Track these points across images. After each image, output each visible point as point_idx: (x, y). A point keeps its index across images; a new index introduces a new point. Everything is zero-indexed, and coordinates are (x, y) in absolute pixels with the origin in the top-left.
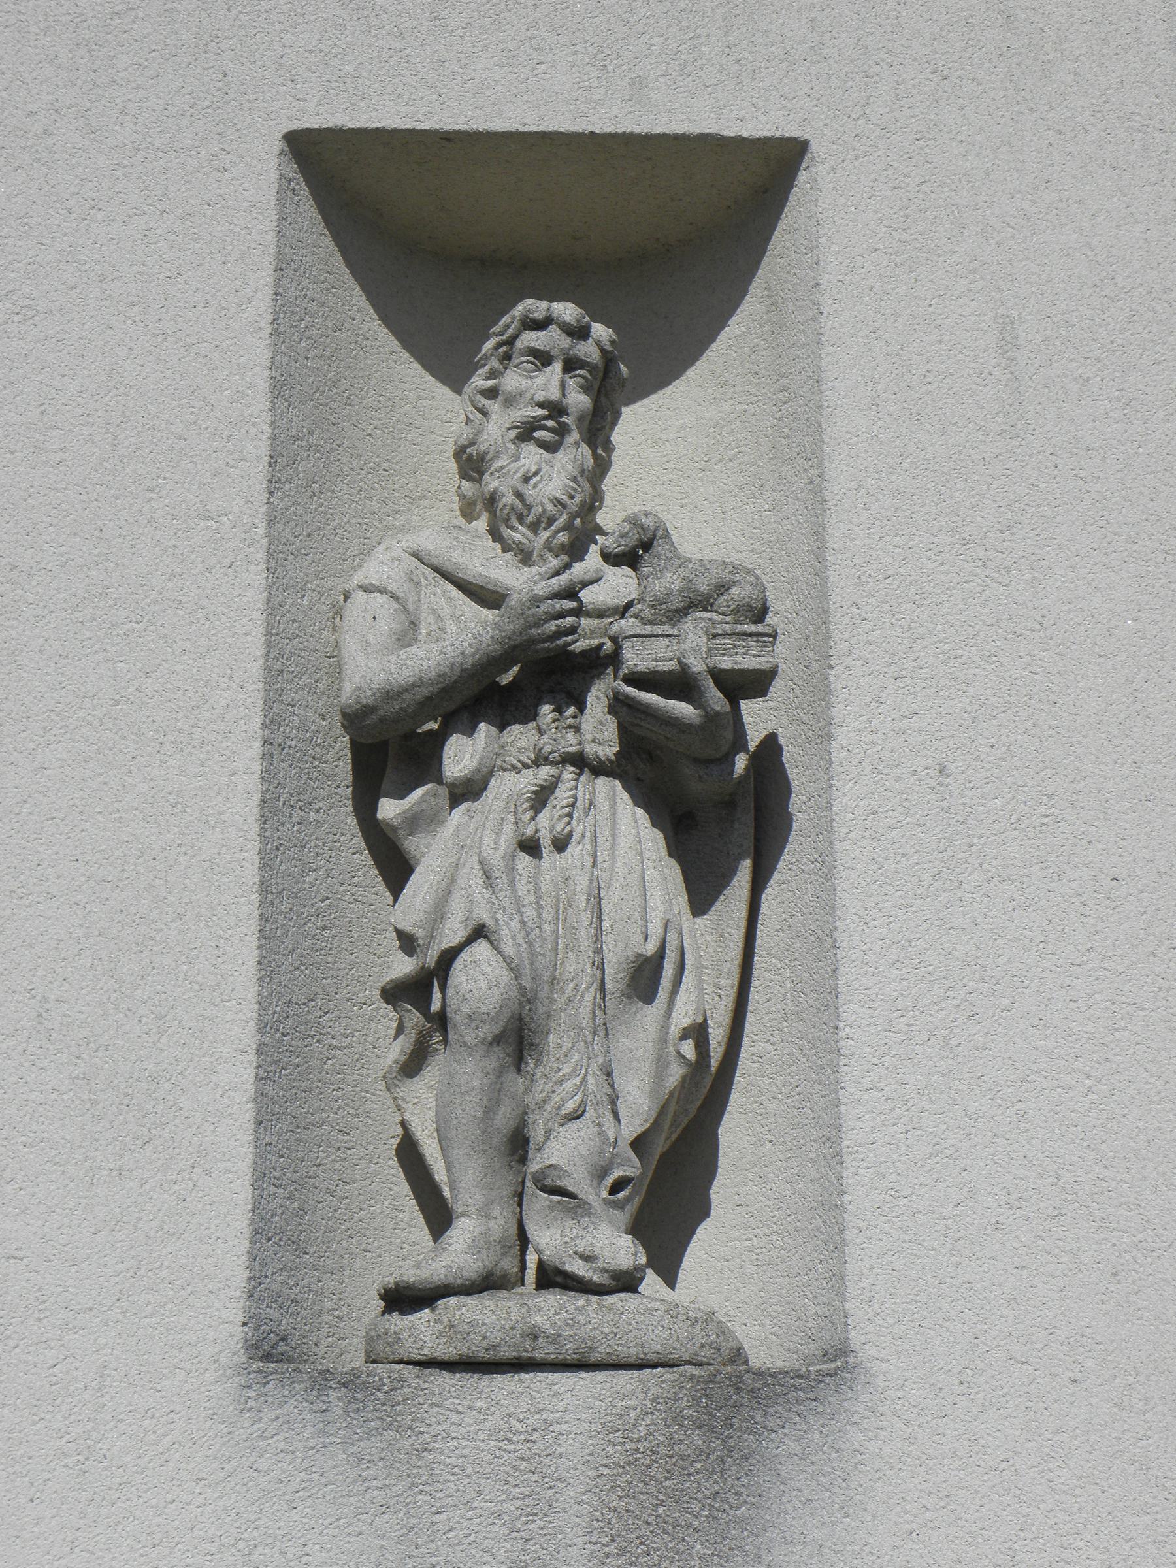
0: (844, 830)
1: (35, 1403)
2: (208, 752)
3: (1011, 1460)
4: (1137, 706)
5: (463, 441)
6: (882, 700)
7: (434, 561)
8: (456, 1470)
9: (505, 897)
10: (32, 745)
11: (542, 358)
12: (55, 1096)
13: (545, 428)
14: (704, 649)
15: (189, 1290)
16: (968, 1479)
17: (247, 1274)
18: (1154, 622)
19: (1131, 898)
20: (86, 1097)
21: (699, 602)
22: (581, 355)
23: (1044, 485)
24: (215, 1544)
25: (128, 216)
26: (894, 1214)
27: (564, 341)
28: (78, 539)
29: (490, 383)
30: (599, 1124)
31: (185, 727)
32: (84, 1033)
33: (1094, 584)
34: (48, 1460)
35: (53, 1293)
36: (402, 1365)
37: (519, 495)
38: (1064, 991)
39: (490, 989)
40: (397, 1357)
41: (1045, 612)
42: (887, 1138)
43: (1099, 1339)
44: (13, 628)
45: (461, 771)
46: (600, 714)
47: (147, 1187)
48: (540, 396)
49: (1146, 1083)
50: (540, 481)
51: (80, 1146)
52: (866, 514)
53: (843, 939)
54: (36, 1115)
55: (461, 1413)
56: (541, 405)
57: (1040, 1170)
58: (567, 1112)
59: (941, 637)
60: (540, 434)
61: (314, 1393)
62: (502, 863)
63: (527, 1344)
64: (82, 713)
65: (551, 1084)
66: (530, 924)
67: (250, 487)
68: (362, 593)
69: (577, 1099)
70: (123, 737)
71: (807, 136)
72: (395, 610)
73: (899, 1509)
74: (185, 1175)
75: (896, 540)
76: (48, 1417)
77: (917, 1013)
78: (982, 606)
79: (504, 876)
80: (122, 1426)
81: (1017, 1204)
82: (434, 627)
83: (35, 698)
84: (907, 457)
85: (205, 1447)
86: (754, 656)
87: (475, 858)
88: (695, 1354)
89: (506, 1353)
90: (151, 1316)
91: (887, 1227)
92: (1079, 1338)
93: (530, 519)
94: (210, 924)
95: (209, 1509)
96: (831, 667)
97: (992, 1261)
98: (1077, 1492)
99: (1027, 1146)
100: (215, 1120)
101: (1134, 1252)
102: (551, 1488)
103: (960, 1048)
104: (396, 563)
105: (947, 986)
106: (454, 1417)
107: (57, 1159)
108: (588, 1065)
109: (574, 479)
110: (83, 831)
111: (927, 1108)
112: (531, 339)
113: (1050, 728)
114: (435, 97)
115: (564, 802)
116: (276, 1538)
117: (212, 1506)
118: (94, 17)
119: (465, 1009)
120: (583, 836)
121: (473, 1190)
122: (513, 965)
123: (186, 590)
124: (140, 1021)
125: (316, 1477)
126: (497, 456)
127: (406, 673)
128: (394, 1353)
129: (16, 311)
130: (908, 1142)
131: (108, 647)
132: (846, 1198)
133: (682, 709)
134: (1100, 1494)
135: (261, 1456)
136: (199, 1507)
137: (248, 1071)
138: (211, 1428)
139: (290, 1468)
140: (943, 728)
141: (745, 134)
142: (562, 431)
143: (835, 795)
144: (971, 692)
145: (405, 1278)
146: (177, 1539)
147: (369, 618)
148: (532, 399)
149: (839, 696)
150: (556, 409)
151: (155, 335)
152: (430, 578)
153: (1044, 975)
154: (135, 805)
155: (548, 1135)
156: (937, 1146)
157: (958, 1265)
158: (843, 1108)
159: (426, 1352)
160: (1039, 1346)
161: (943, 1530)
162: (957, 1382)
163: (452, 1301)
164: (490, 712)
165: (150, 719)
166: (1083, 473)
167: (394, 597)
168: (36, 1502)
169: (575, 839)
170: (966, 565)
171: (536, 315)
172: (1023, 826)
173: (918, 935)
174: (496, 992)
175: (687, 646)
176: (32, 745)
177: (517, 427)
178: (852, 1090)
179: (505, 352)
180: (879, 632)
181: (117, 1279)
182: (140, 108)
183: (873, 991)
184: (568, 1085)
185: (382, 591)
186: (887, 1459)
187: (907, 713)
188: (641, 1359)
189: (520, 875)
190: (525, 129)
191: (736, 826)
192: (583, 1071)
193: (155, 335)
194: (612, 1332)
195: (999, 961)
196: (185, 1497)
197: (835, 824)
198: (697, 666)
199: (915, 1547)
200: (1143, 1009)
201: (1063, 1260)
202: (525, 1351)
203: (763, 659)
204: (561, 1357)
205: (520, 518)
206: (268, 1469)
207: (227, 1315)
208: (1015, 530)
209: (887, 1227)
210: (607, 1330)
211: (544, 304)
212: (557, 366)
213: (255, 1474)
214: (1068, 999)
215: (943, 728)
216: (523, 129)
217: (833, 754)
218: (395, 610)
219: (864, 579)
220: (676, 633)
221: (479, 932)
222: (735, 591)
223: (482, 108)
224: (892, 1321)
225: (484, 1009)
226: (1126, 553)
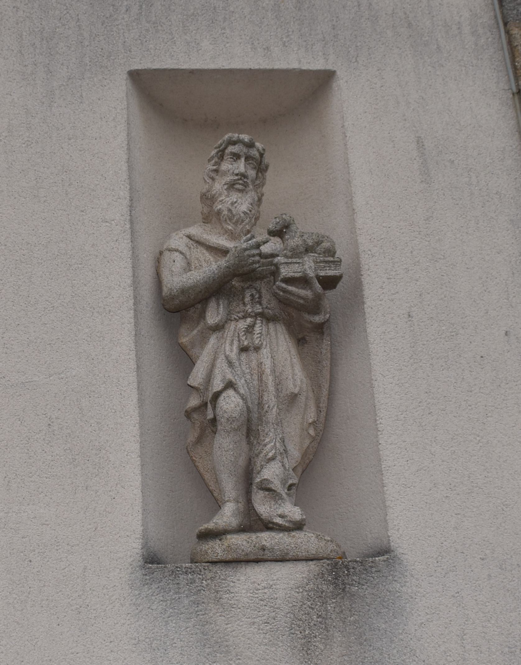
0: (373, 340)
1: (58, 584)
2: (112, 315)
3: (460, 593)
4: (485, 288)
5: (204, 191)
6: (384, 287)
7: (196, 238)
8: (234, 606)
9: (238, 370)
10: (40, 315)
11: (236, 157)
12: (58, 457)
13: (240, 184)
14: (313, 268)
15: (119, 535)
16: (443, 601)
17: (142, 528)
18: (488, 255)
19: (489, 364)
20: (70, 457)
21: (308, 250)
22: (252, 155)
23: (440, 202)
24: (137, 640)
25: (67, 104)
26: (405, 494)
27: (245, 150)
28: (54, 232)
29: (215, 167)
30: (282, 462)
31: (102, 305)
32: (69, 431)
33: (463, 240)
34: (64, 608)
35: (62, 539)
36: (209, 564)
37: (230, 210)
38: (465, 402)
39: (236, 407)
40: (206, 560)
41: (445, 251)
42: (400, 464)
43: (491, 542)
44: (29, 268)
45: (214, 321)
46: (269, 297)
47: (98, 494)
48: (236, 171)
49: (501, 438)
50: (237, 205)
51: (69, 478)
52: (371, 214)
53: (376, 384)
54: (50, 465)
55: (234, 582)
56: (237, 175)
57: (462, 474)
58: (269, 457)
59: (405, 262)
60: (237, 186)
61: (173, 576)
62: (235, 357)
63: (261, 552)
64: (59, 301)
65: (261, 446)
66: (248, 381)
67: (122, 209)
68: (168, 252)
69: (273, 451)
70: (77, 311)
71: (335, 69)
72: (182, 258)
73: (416, 614)
74: (113, 488)
75: (384, 225)
76: (63, 590)
77: (407, 413)
78: (420, 250)
79: (237, 362)
80: (94, 593)
81: (454, 489)
82: (198, 265)
83: (40, 296)
84: (385, 192)
85: (129, 600)
86: (333, 270)
87: (223, 356)
88: (329, 555)
89: (252, 557)
90: (103, 547)
91: (403, 500)
92: (483, 542)
93: (234, 221)
94: (118, 385)
95: (133, 626)
96: (362, 275)
97: (446, 512)
98: (487, 604)
99: (456, 465)
100: (124, 465)
101: (502, 506)
102: (274, 612)
103: (426, 426)
104: (181, 240)
105: (419, 402)
106: (232, 584)
107: (60, 483)
108: (276, 438)
109: (251, 204)
110: (62, 349)
111: (415, 451)
112: (231, 149)
113: (451, 297)
114: (187, 56)
115: (258, 332)
116: (161, 637)
117: (134, 625)
118: (49, 28)
119: (226, 415)
120: (266, 345)
121: (231, 491)
122: (244, 397)
123: (99, 251)
124: (91, 425)
125: (176, 611)
126: (220, 195)
127: (190, 281)
128: (205, 559)
129: (24, 142)
130: (409, 465)
131: (69, 274)
132: (385, 488)
133: (303, 292)
134: (496, 605)
135: (153, 603)
136: (128, 625)
137: (137, 444)
138: (131, 592)
139: (165, 608)
140: (409, 298)
141: (311, 68)
142: (246, 185)
143: (368, 326)
144: (418, 283)
145: (209, 527)
146: (120, 639)
147: (172, 261)
148: (233, 173)
149: (366, 287)
150: (244, 176)
151: (80, 151)
152: (195, 246)
153: (457, 396)
154: (84, 337)
155: (262, 467)
156: (420, 466)
157: (432, 514)
158: (381, 452)
159: (219, 557)
160: (467, 546)
161: (434, 622)
162: (435, 562)
163: (229, 536)
164: (224, 298)
165: (88, 303)
166: (455, 197)
167: (181, 253)
168: (60, 625)
169: (264, 346)
170: (412, 234)
171: (234, 139)
172: (444, 336)
173: (406, 381)
174: (238, 409)
175: (306, 267)
176: (40, 315)
177: (227, 184)
178: (384, 445)
179: (220, 155)
180: (380, 261)
181: (88, 532)
182: (69, 63)
183: (389, 404)
184: (269, 446)
185: (177, 250)
186: (410, 594)
187: (393, 293)
188: (307, 557)
189: (243, 362)
190: (224, 68)
191: (324, 341)
192: (274, 440)
193: (80, 151)
194: (295, 547)
195: (439, 391)
196: (123, 621)
197: (368, 338)
198: (311, 274)
199: (424, 629)
200: (497, 408)
201: (474, 510)
202: (260, 556)
203: (337, 271)
204: (274, 558)
205: (230, 220)
206: (156, 608)
207: (134, 545)
208: (430, 220)
209: (403, 500)
210: (293, 546)
211: (236, 135)
212: (243, 160)
213: (151, 611)
214: (467, 405)
215: (409, 298)
216: (222, 68)
217: (366, 310)
218: (182, 258)
219: (372, 240)
220: (301, 261)
221: (230, 385)
222: (324, 244)
223: (206, 60)
224: (408, 538)
225: (234, 415)
226: (474, 228)
